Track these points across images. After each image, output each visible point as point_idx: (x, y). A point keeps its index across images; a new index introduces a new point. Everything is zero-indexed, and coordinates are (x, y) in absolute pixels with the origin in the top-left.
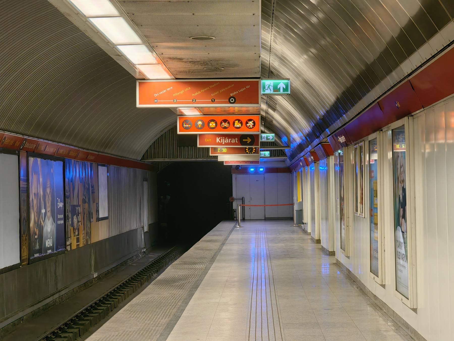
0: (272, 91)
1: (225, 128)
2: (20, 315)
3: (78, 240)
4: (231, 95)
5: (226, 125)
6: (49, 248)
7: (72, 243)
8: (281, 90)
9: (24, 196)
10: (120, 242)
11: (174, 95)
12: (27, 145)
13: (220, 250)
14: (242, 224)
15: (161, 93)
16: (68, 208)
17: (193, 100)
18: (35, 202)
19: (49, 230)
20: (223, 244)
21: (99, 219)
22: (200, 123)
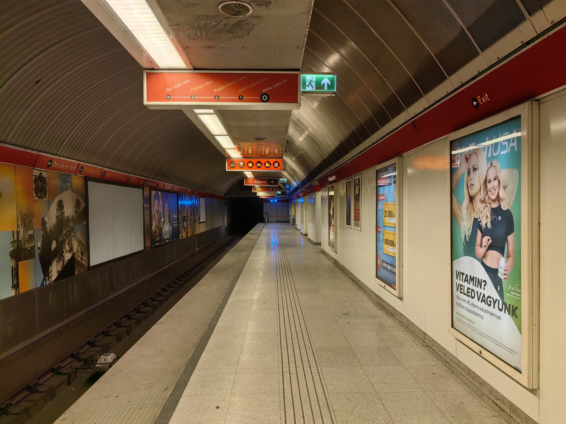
0: (314, 88)
1: (259, 167)
2: (143, 279)
3: (187, 234)
4: (264, 91)
5: (259, 165)
6: (167, 239)
7: (183, 235)
8: (326, 88)
9: (147, 212)
10: (211, 234)
11: (191, 90)
12: (149, 184)
13: (257, 240)
14: (268, 224)
15: (175, 87)
16: (180, 217)
17: (215, 97)
18: (156, 215)
19: (167, 230)
20: (259, 236)
21: (200, 223)
22: (242, 163)
